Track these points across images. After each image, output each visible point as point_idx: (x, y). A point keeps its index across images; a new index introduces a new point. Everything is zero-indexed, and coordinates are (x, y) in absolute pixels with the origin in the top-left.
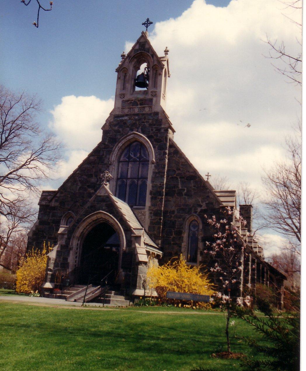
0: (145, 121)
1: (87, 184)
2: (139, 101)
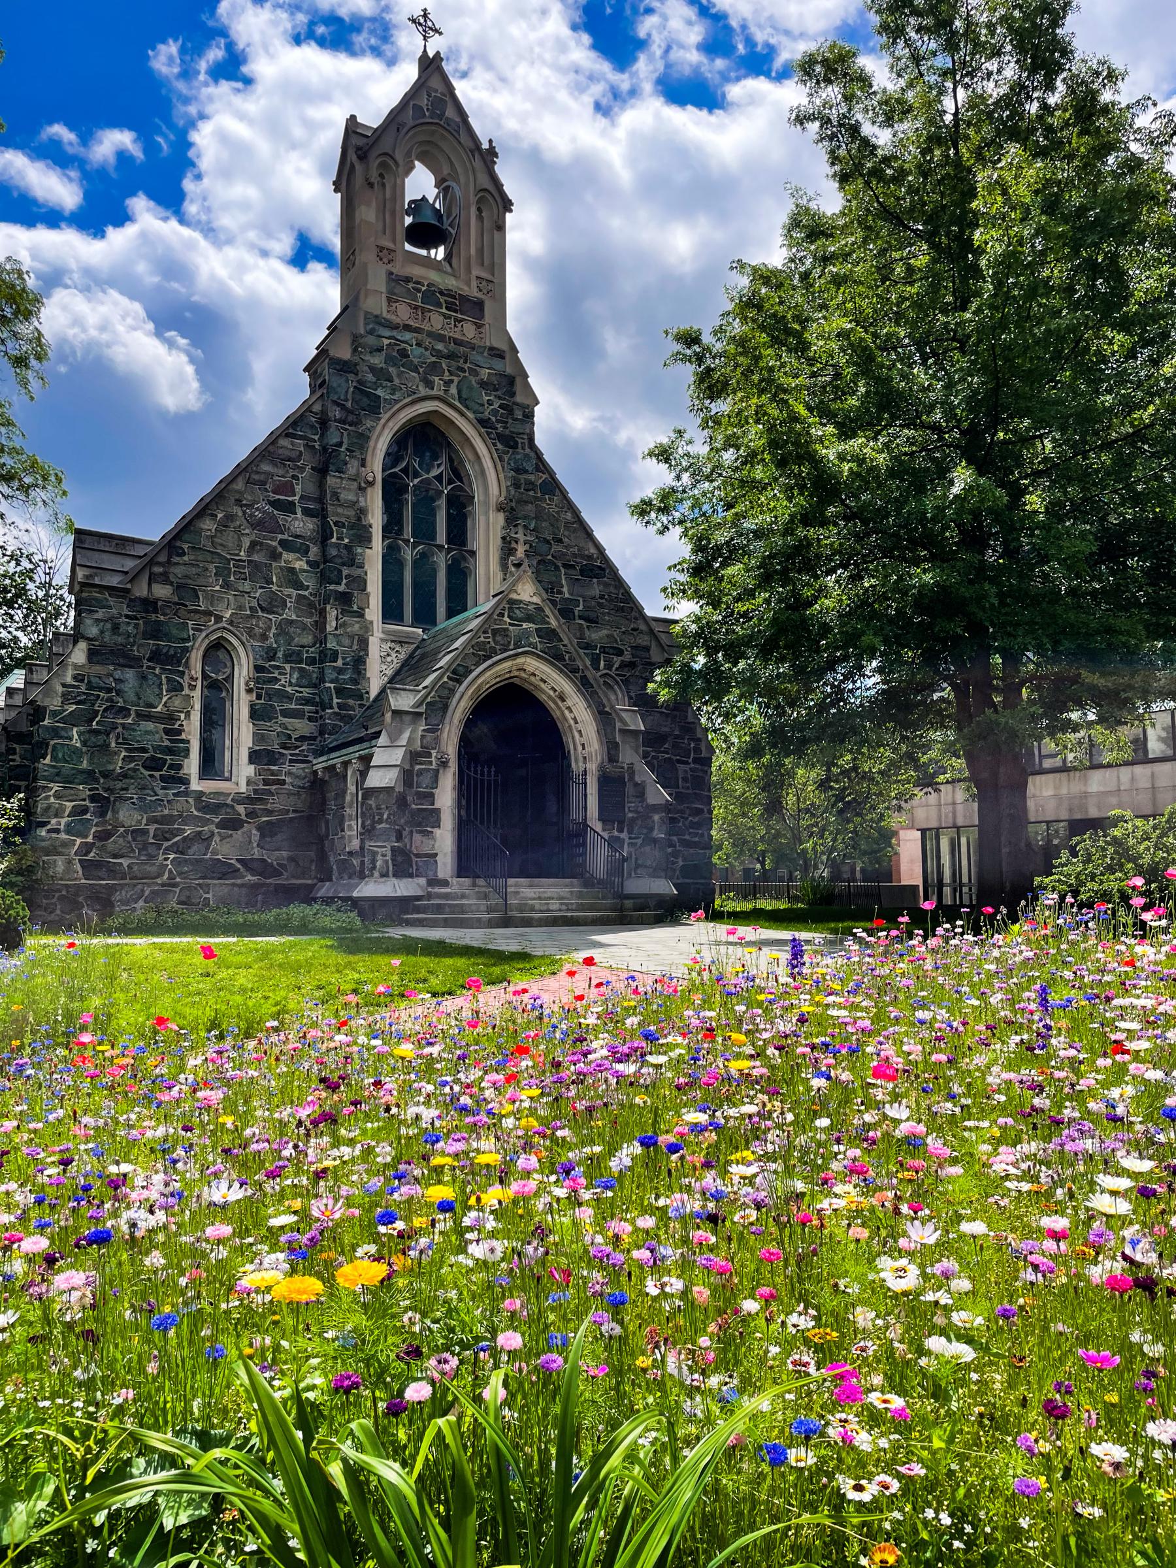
0: (466, 367)
1: (280, 537)
2: (441, 293)
